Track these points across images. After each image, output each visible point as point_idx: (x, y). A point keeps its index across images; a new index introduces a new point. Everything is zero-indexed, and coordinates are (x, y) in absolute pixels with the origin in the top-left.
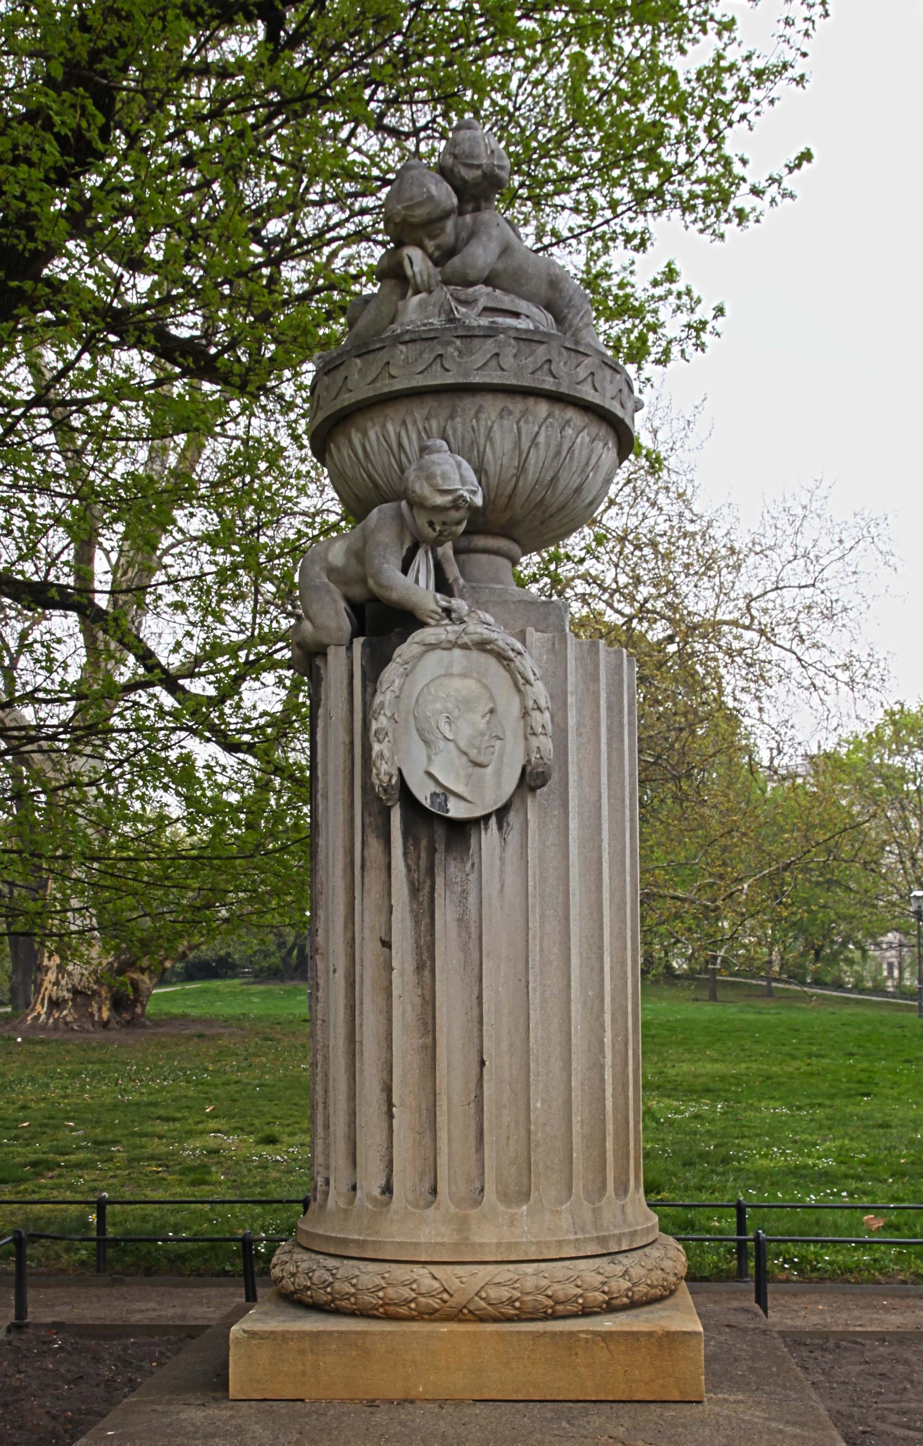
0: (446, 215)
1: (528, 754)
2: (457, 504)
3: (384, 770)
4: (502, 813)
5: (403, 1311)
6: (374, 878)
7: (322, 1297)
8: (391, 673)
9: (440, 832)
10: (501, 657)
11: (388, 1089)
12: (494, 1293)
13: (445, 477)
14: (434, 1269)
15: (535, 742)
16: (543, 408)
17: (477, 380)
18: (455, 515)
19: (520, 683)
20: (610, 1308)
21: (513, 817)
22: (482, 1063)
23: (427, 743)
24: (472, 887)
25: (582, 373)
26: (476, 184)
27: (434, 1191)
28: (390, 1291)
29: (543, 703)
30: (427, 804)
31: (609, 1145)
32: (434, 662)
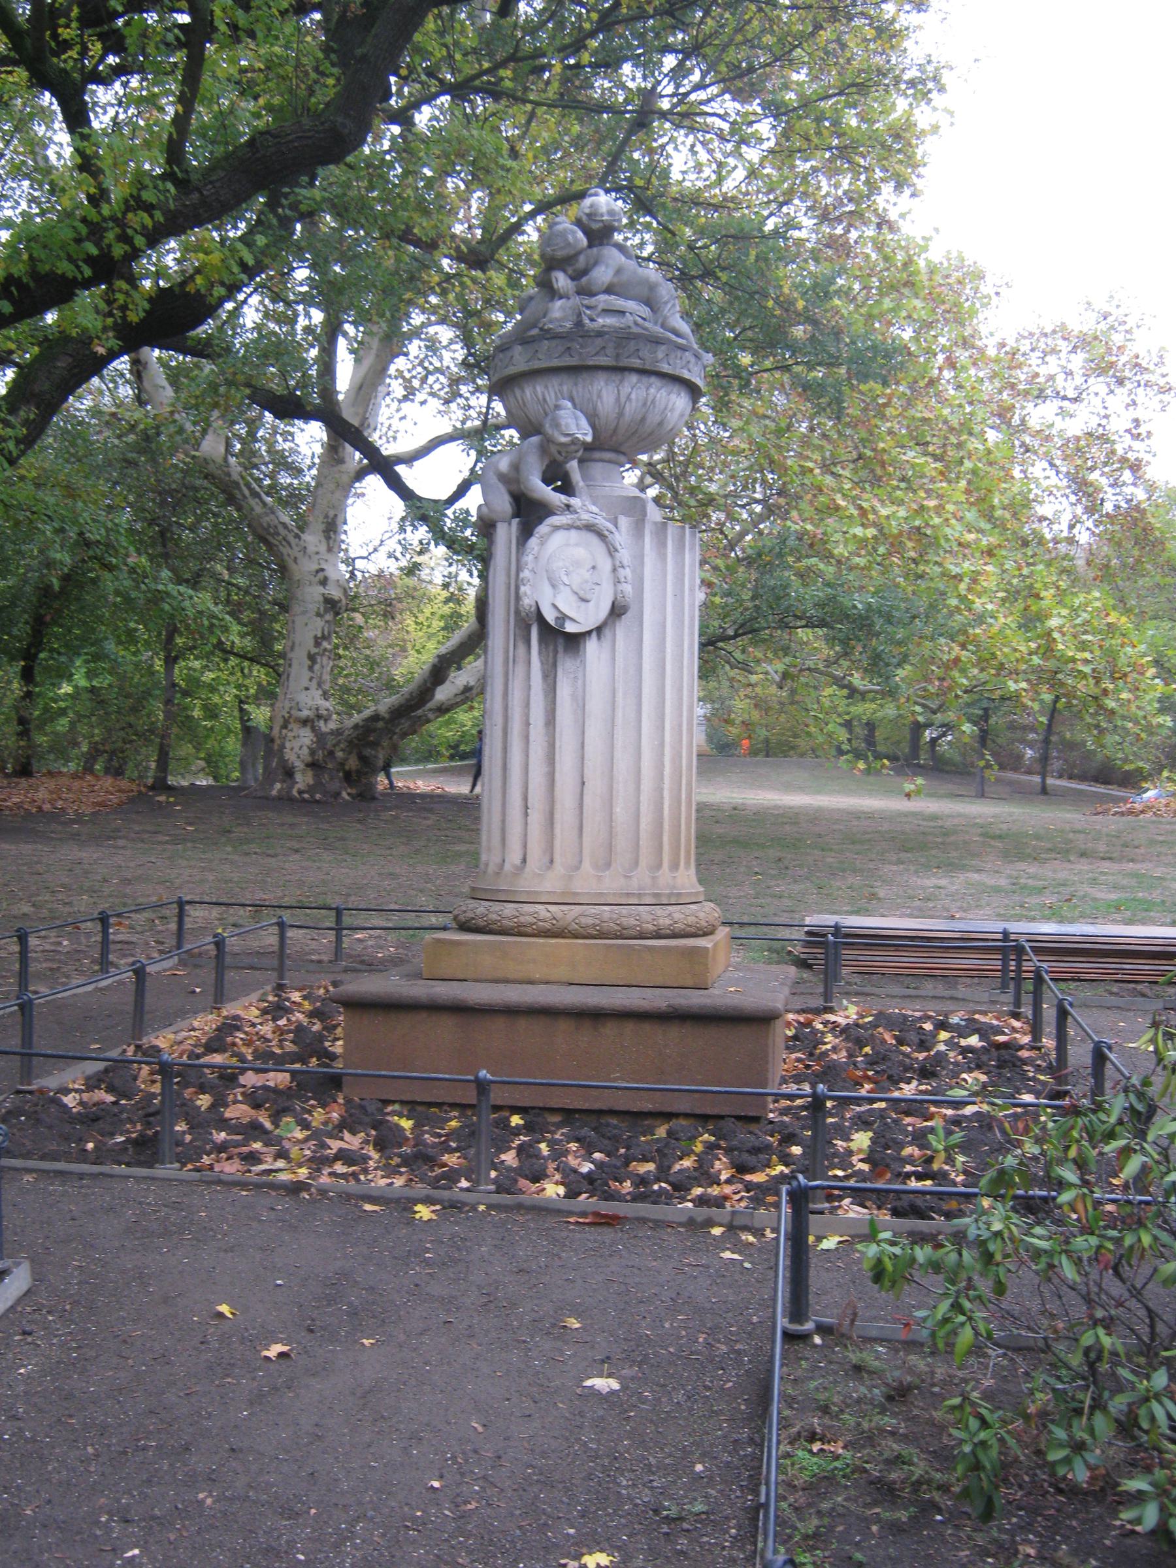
0: (579, 253)
1: (615, 593)
2: (575, 441)
3: (527, 602)
4: (599, 630)
5: (529, 930)
6: (520, 669)
7: (481, 923)
8: (533, 542)
9: (561, 641)
10: (600, 535)
11: (525, 799)
12: (584, 920)
13: (567, 425)
14: (550, 907)
15: (620, 587)
16: (634, 378)
17: (591, 363)
18: (573, 448)
19: (612, 551)
20: (658, 936)
21: (607, 632)
22: (583, 783)
23: (554, 586)
24: (580, 675)
25: (660, 355)
26: (599, 230)
27: (552, 861)
28: (522, 919)
29: (625, 563)
30: (552, 623)
31: (666, 839)
32: (559, 538)
